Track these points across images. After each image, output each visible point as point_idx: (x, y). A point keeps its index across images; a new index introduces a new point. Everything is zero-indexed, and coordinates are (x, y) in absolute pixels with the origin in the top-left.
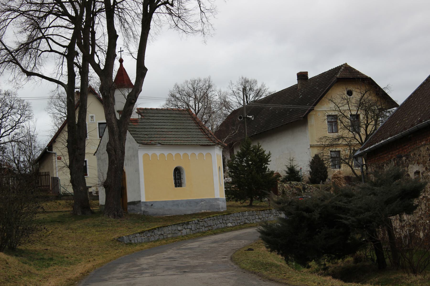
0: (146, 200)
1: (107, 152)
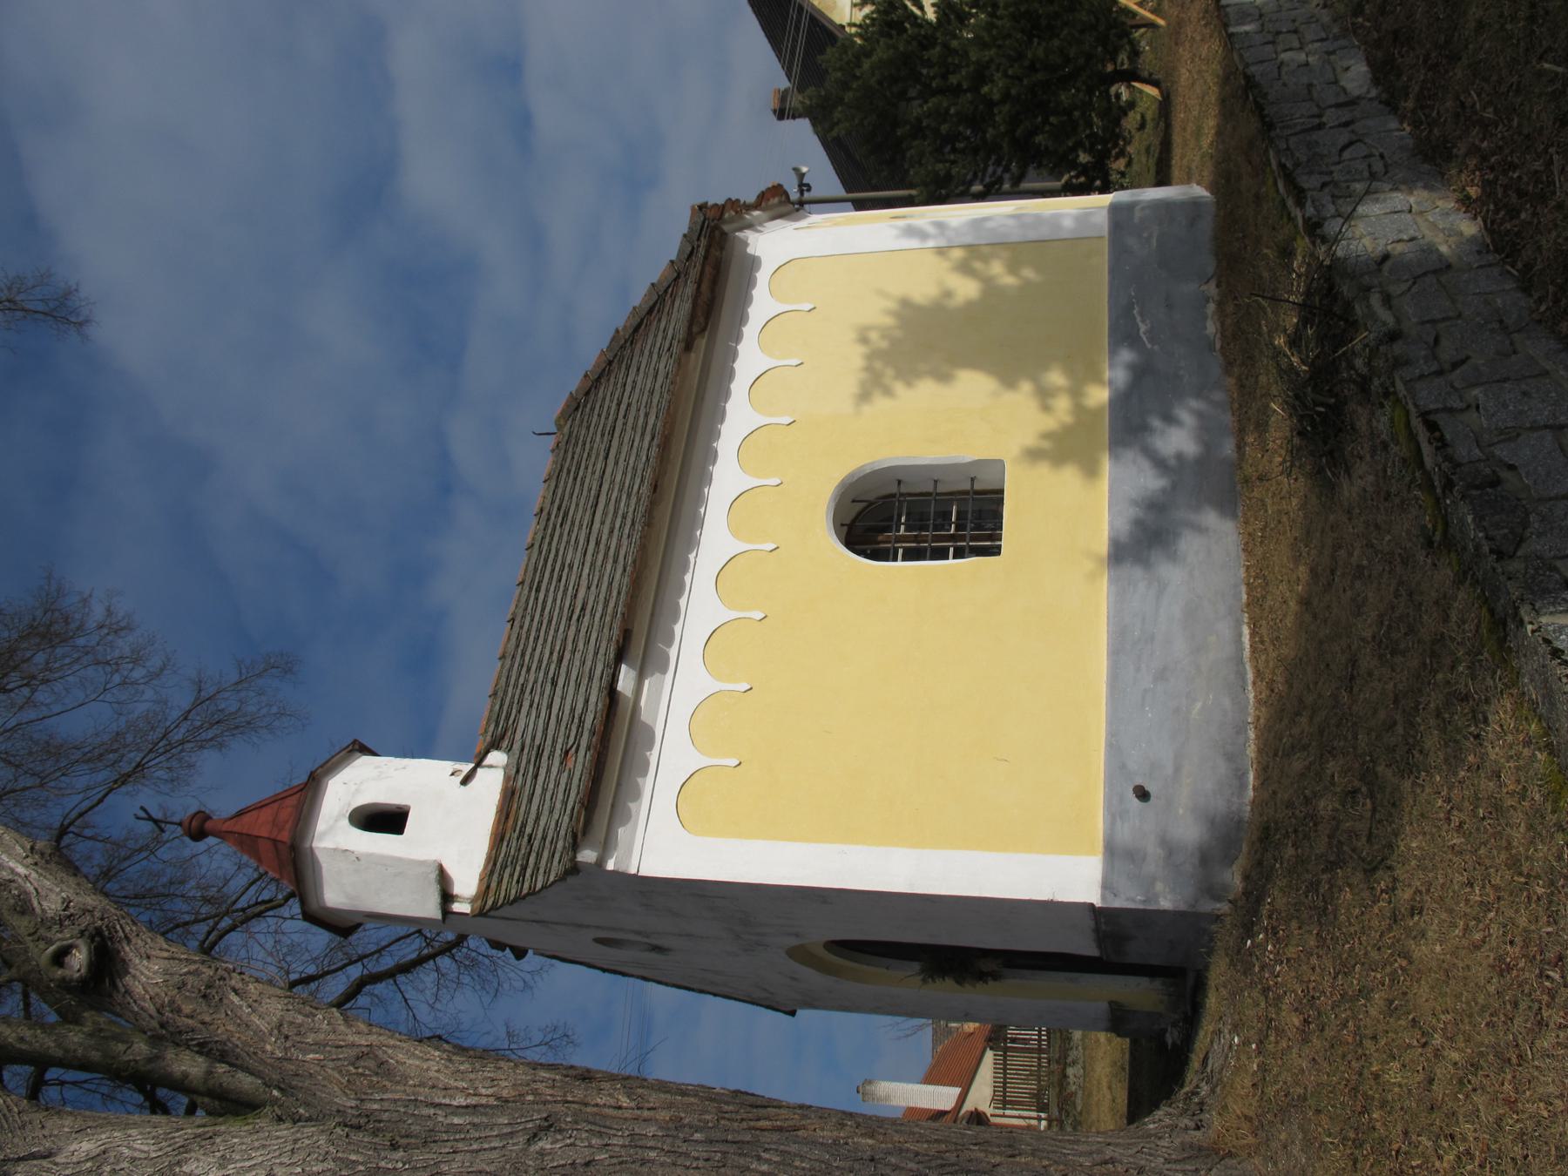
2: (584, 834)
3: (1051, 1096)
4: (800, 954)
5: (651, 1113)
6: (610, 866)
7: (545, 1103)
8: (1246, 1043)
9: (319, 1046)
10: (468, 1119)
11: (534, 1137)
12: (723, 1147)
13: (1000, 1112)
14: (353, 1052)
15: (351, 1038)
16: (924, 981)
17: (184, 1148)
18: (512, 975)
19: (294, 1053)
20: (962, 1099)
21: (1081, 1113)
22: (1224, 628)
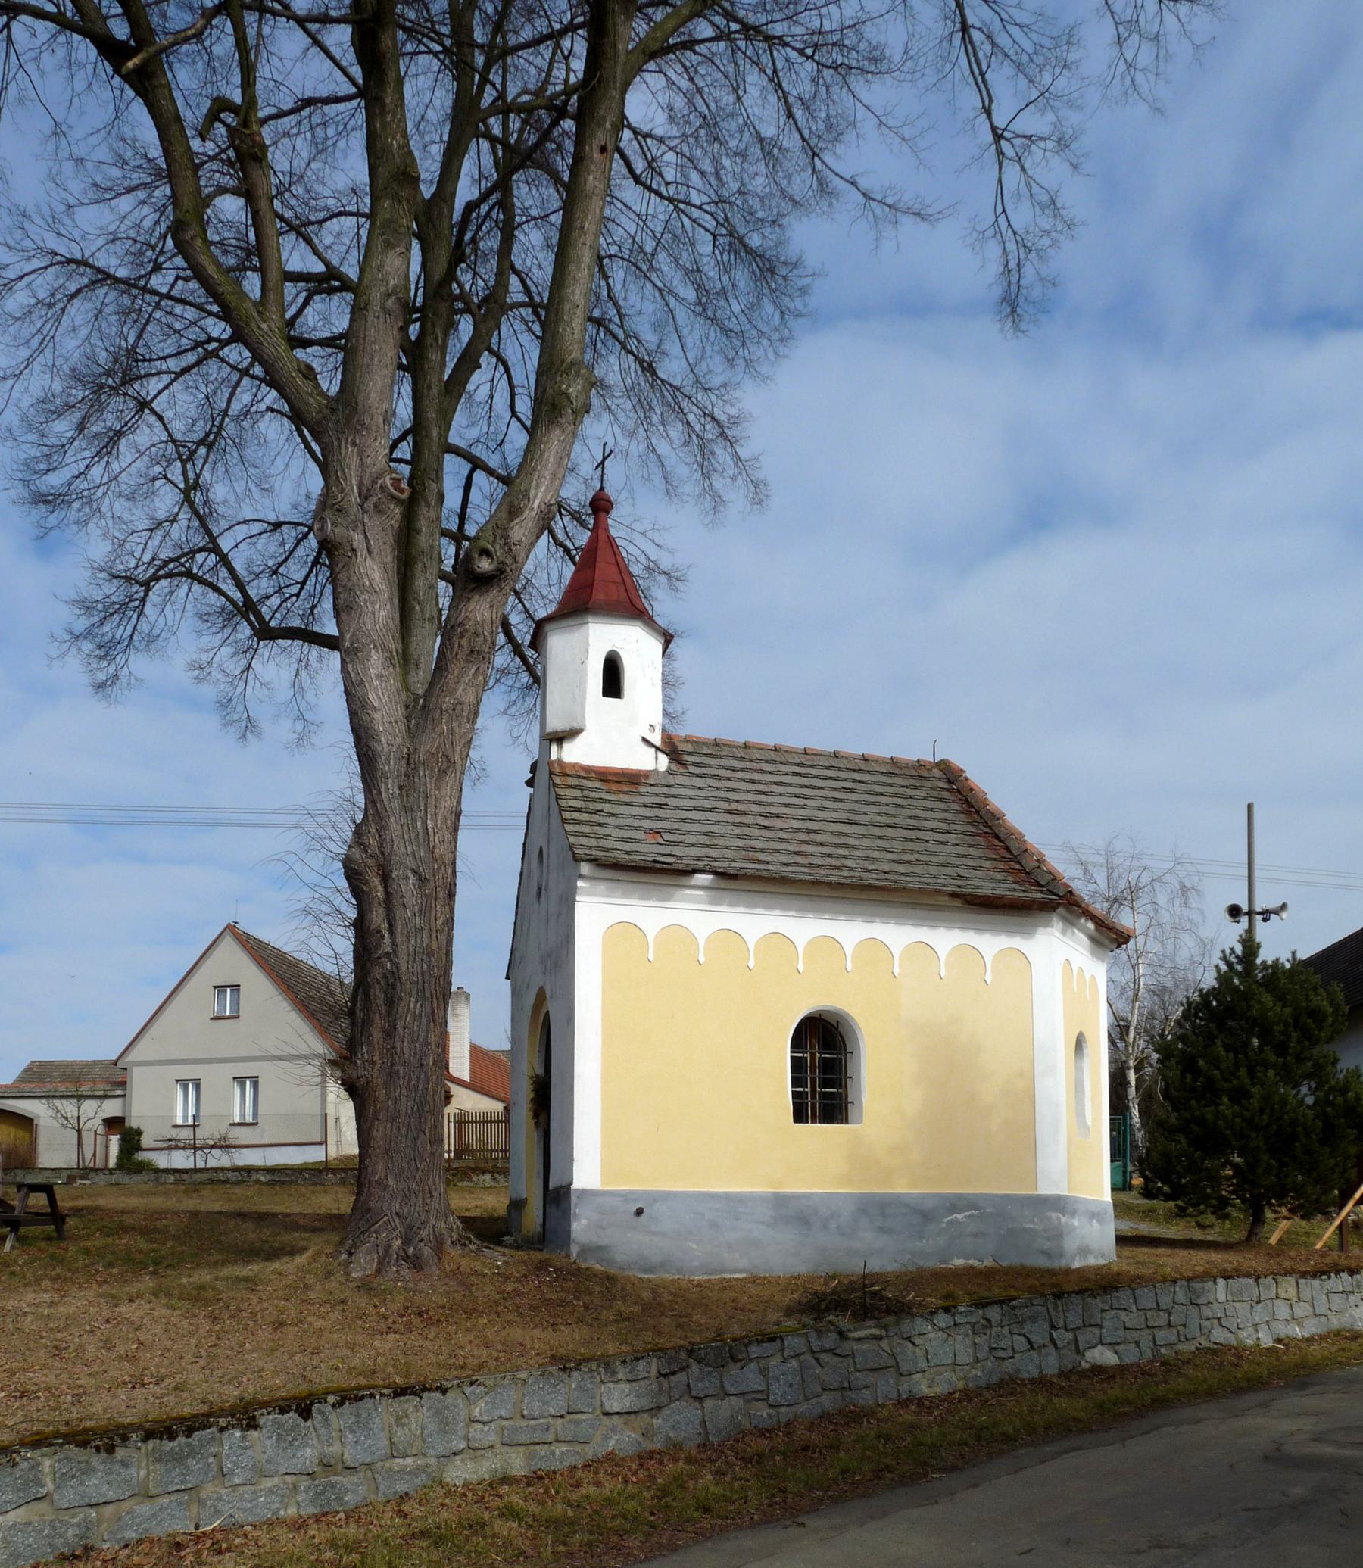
0: (603, 1183)
1: (350, 885)
2: (598, 865)
3: (467, 1161)
4: (541, 998)
5: (434, 938)
6: (580, 883)
7: (434, 876)
8: (498, 1267)
9: (451, 731)
10: (421, 831)
11: (415, 872)
12: (420, 982)
13: (452, 1119)
14: (450, 754)
15: (458, 749)
16: (531, 1077)
17: (384, 647)
18: (523, 726)
19: (446, 716)
20: (460, 1083)
21: (455, 1185)
22: (743, 1263)
